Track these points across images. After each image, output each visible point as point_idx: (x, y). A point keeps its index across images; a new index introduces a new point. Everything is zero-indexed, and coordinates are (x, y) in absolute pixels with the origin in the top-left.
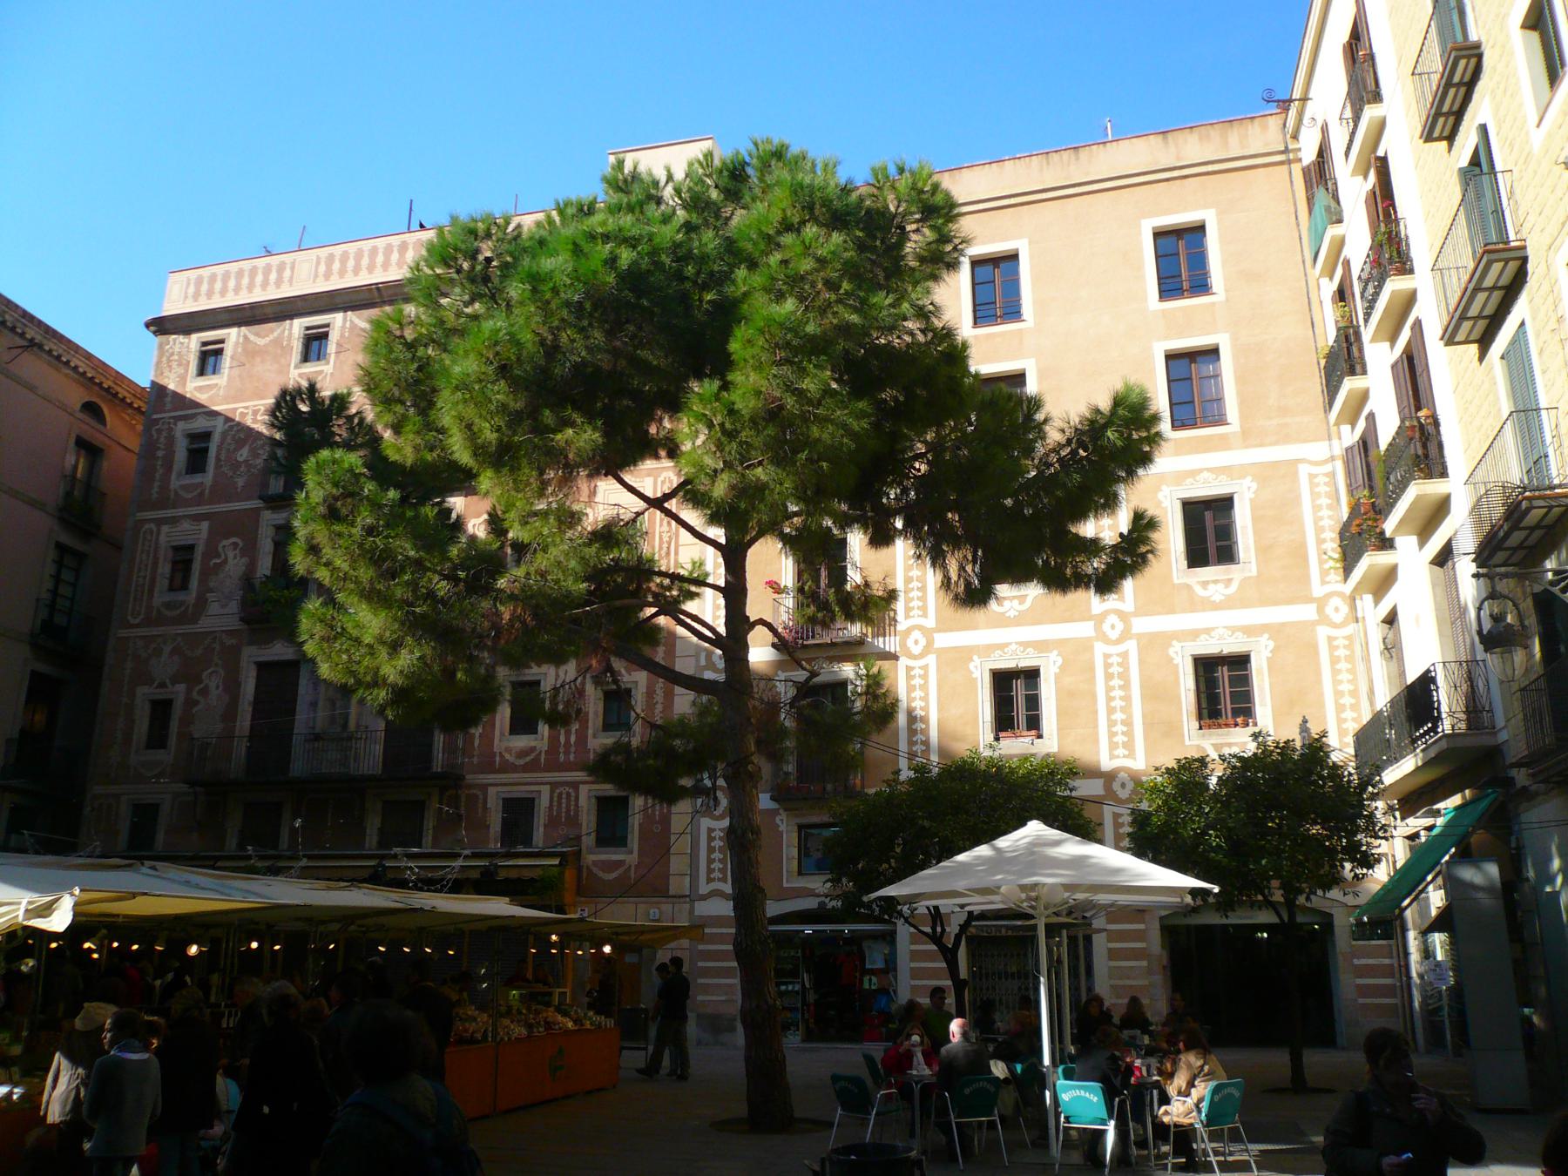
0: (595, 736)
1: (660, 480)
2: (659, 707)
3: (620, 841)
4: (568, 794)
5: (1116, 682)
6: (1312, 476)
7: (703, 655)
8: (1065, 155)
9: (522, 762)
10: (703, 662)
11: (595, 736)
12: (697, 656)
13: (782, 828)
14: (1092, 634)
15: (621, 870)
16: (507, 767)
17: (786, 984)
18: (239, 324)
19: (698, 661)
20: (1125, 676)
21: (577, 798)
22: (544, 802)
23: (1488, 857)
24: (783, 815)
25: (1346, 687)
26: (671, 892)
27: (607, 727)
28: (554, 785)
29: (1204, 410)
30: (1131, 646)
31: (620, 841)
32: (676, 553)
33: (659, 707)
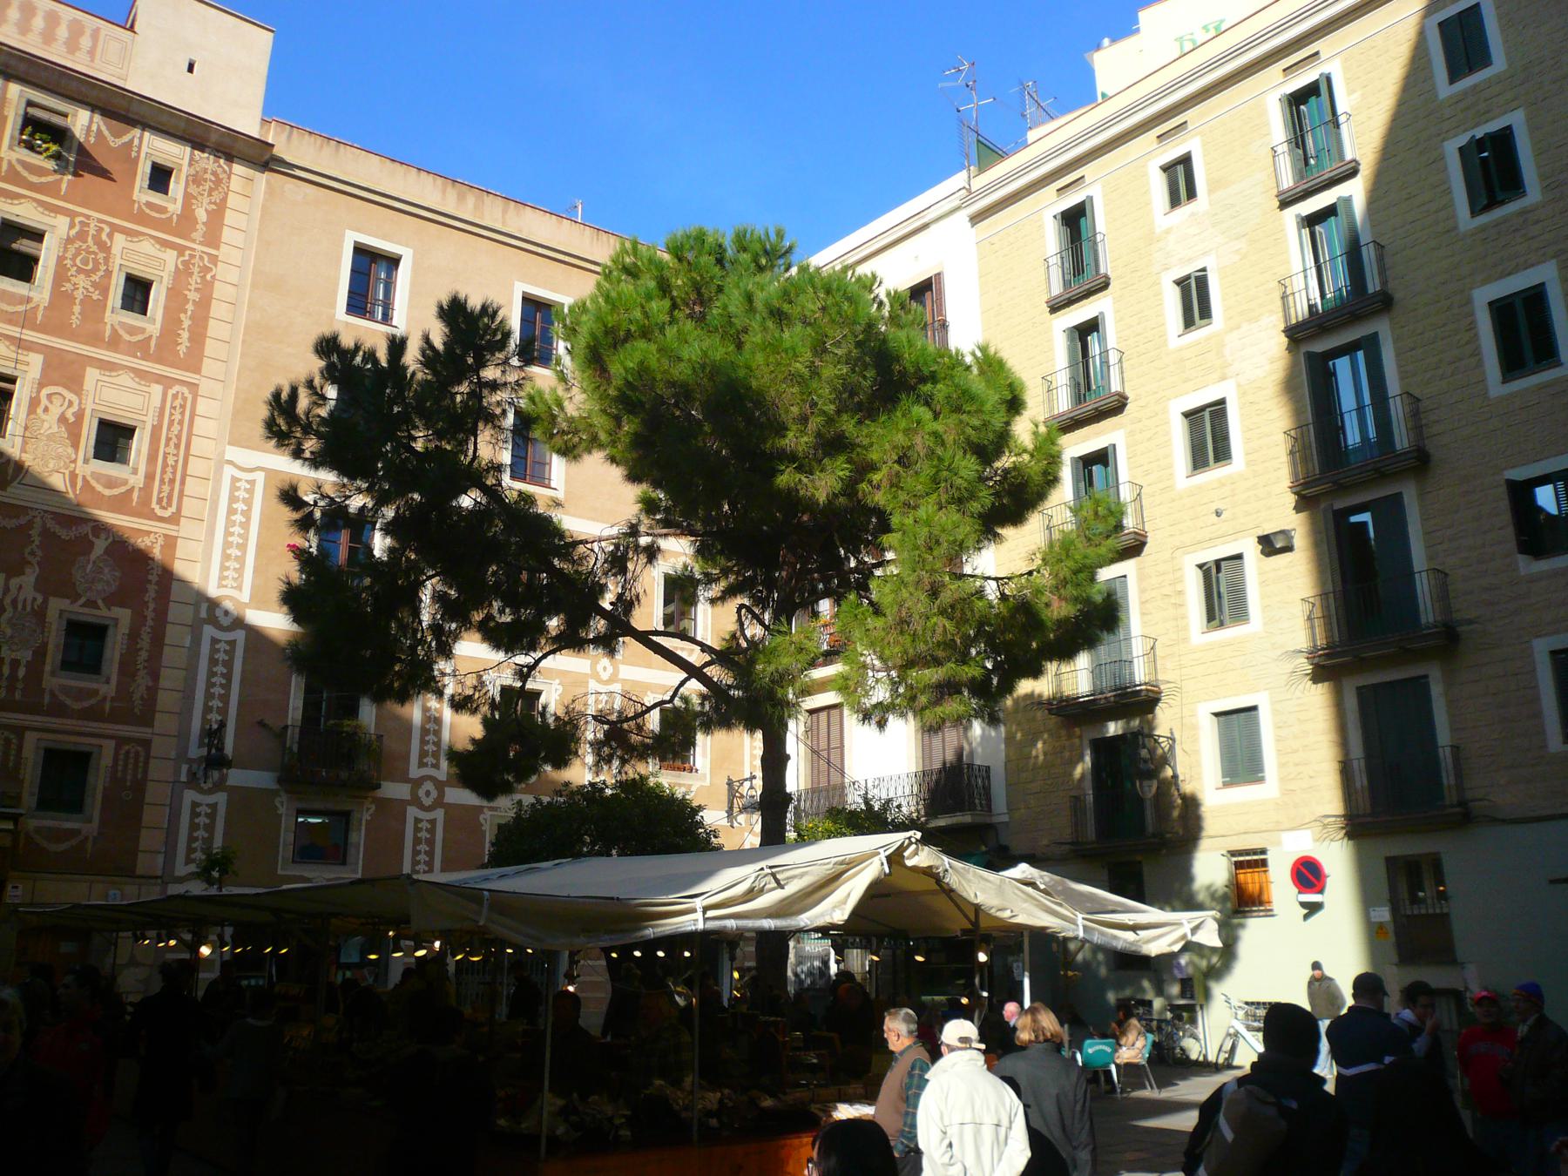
0: (53, 674)
1: (171, 392)
2: (144, 655)
3: (76, 806)
4: (137, 753)
5: (220, 669)
6: (234, 480)
7: (204, 606)
8: (440, 180)
9: (77, 706)
10: (203, 614)
11: (53, 674)
12: (197, 605)
13: (282, 810)
14: (588, 671)
15: (74, 842)
16: (58, 710)
17: (248, 978)
18: (94, 108)
19: (197, 611)
20: (229, 664)
21: (20, 747)
22: (106, 760)
23: (1409, 911)
24: (284, 797)
25: (217, 690)
26: (140, 871)
27: (66, 665)
28: (121, 741)
29: (533, 469)
30: (439, 814)
31: (76, 806)
32: (183, 483)
33: (144, 655)
